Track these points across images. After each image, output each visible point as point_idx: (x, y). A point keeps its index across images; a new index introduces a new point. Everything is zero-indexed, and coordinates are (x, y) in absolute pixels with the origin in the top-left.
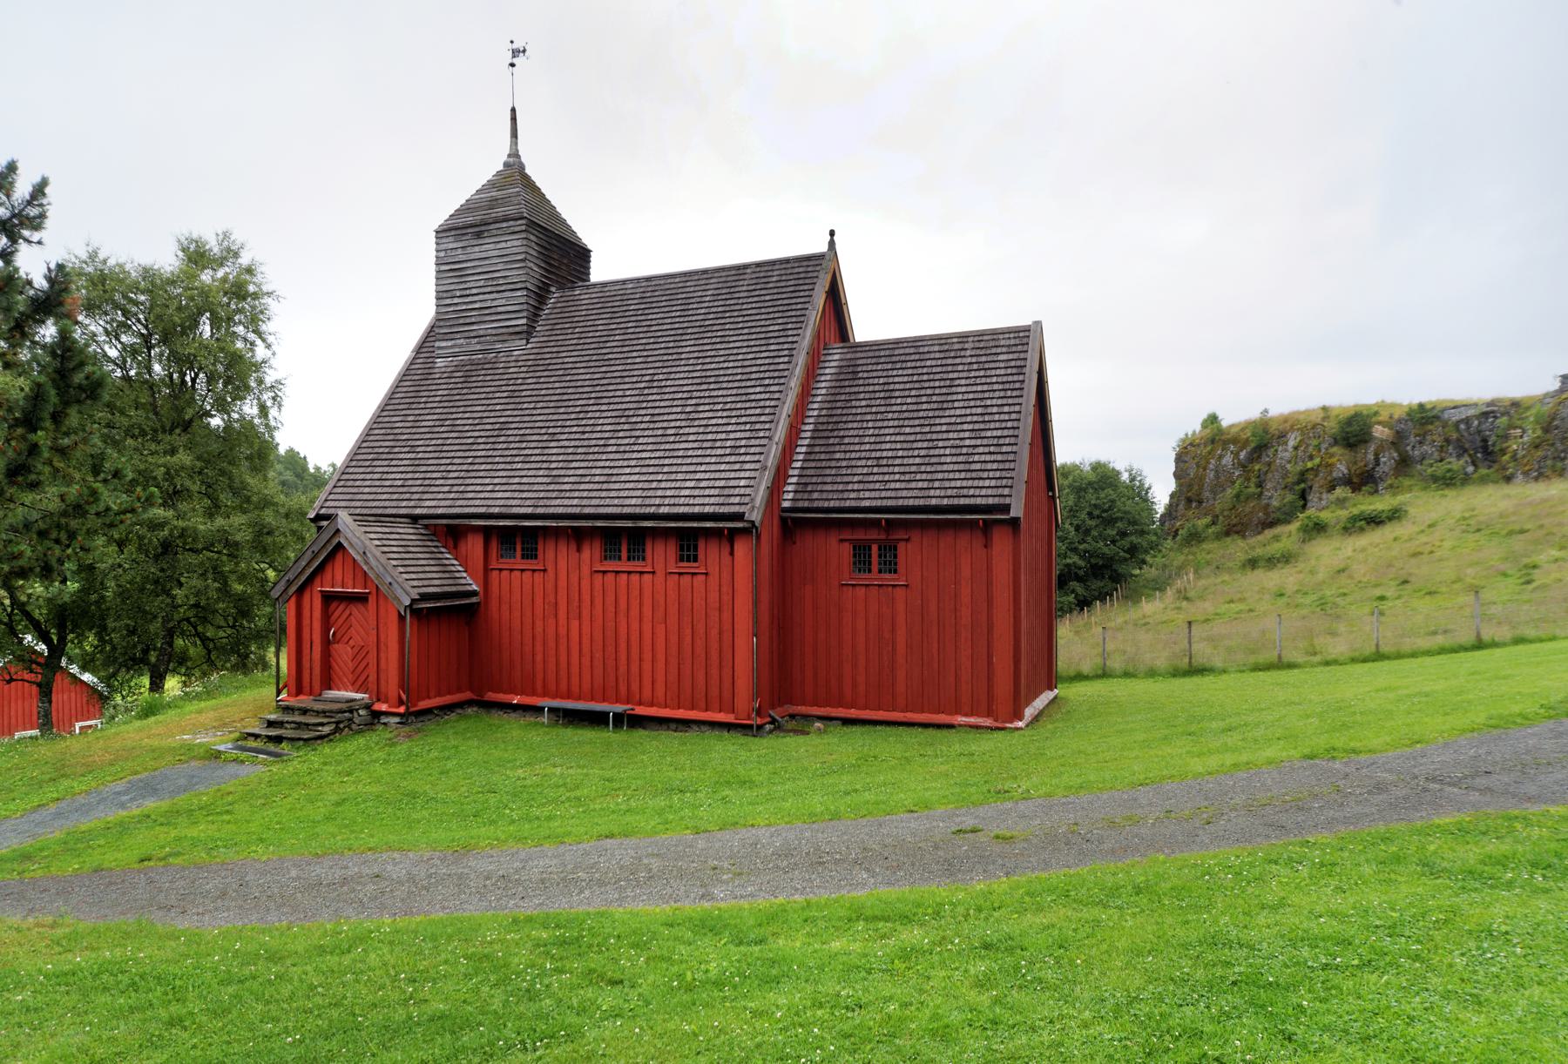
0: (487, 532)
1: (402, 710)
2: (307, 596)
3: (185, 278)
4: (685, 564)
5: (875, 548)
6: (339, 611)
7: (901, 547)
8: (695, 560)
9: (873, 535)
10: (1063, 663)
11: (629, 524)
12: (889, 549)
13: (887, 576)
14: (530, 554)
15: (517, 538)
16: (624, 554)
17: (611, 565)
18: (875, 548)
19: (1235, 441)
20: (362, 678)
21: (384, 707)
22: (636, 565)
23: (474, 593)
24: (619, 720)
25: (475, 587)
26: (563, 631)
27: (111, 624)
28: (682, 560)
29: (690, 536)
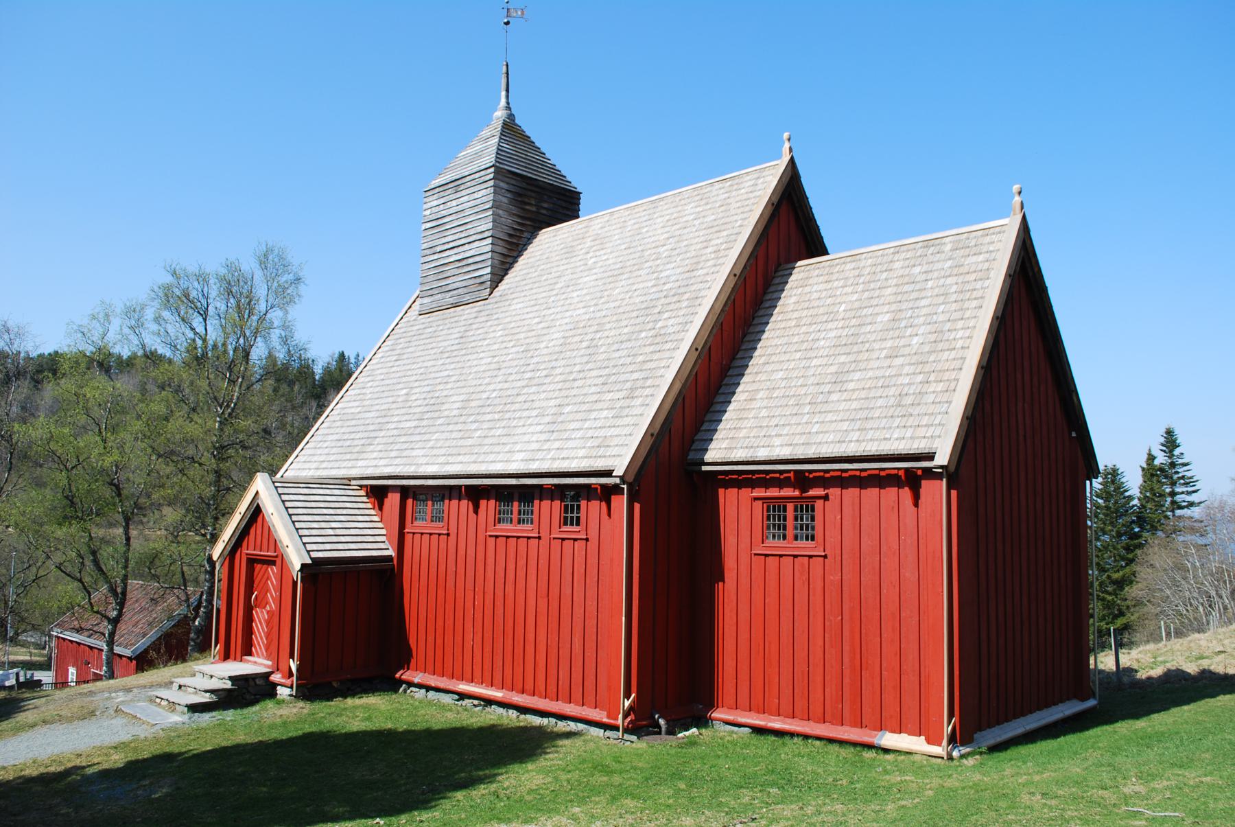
4: (568, 528)
5: (790, 507)
12: (806, 506)
13: (802, 543)
16: (515, 516)
18: (790, 507)
22: (526, 529)
23: (389, 558)
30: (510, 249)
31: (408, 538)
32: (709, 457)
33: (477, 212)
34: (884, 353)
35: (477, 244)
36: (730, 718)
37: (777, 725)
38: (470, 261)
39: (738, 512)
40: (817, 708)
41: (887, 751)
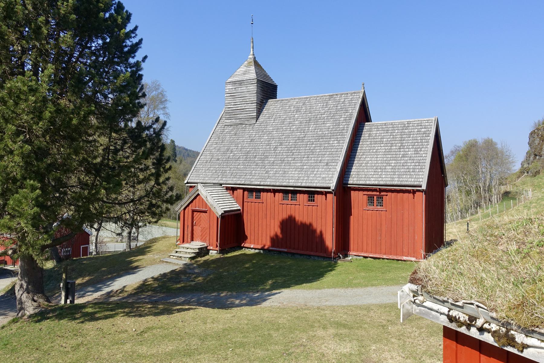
0: (244, 189)
2: (187, 209)
4: (310, 202)
5: (375, 197)
6: (195, 213)
7: (384, 197)
8: (314, 201)
10: (448, 237)
11: (292, 189)
12: (380, 197)
13: (379, 207)
14: (258, 197)
15: (256, 191)
16: (290, 198)
17: (285, 202)
18: (375, 197)
20: (204, 238)
21: (211, 248)
22: (294, 202)
23: (239, 210)
24: (287, 253)
27: (119, 213)
28: (309, 201)
29: (312, 193)
30: (261, 105)
31: (245, 203)
32: (350, 182)
33: (251, 92)
34: (401, 156)
35: (250, 105)
36: (357, 254)
37: (395, 258)
38: (247, 110)
39: (358, 199)
40: (384, 251)
41: (405, 261)
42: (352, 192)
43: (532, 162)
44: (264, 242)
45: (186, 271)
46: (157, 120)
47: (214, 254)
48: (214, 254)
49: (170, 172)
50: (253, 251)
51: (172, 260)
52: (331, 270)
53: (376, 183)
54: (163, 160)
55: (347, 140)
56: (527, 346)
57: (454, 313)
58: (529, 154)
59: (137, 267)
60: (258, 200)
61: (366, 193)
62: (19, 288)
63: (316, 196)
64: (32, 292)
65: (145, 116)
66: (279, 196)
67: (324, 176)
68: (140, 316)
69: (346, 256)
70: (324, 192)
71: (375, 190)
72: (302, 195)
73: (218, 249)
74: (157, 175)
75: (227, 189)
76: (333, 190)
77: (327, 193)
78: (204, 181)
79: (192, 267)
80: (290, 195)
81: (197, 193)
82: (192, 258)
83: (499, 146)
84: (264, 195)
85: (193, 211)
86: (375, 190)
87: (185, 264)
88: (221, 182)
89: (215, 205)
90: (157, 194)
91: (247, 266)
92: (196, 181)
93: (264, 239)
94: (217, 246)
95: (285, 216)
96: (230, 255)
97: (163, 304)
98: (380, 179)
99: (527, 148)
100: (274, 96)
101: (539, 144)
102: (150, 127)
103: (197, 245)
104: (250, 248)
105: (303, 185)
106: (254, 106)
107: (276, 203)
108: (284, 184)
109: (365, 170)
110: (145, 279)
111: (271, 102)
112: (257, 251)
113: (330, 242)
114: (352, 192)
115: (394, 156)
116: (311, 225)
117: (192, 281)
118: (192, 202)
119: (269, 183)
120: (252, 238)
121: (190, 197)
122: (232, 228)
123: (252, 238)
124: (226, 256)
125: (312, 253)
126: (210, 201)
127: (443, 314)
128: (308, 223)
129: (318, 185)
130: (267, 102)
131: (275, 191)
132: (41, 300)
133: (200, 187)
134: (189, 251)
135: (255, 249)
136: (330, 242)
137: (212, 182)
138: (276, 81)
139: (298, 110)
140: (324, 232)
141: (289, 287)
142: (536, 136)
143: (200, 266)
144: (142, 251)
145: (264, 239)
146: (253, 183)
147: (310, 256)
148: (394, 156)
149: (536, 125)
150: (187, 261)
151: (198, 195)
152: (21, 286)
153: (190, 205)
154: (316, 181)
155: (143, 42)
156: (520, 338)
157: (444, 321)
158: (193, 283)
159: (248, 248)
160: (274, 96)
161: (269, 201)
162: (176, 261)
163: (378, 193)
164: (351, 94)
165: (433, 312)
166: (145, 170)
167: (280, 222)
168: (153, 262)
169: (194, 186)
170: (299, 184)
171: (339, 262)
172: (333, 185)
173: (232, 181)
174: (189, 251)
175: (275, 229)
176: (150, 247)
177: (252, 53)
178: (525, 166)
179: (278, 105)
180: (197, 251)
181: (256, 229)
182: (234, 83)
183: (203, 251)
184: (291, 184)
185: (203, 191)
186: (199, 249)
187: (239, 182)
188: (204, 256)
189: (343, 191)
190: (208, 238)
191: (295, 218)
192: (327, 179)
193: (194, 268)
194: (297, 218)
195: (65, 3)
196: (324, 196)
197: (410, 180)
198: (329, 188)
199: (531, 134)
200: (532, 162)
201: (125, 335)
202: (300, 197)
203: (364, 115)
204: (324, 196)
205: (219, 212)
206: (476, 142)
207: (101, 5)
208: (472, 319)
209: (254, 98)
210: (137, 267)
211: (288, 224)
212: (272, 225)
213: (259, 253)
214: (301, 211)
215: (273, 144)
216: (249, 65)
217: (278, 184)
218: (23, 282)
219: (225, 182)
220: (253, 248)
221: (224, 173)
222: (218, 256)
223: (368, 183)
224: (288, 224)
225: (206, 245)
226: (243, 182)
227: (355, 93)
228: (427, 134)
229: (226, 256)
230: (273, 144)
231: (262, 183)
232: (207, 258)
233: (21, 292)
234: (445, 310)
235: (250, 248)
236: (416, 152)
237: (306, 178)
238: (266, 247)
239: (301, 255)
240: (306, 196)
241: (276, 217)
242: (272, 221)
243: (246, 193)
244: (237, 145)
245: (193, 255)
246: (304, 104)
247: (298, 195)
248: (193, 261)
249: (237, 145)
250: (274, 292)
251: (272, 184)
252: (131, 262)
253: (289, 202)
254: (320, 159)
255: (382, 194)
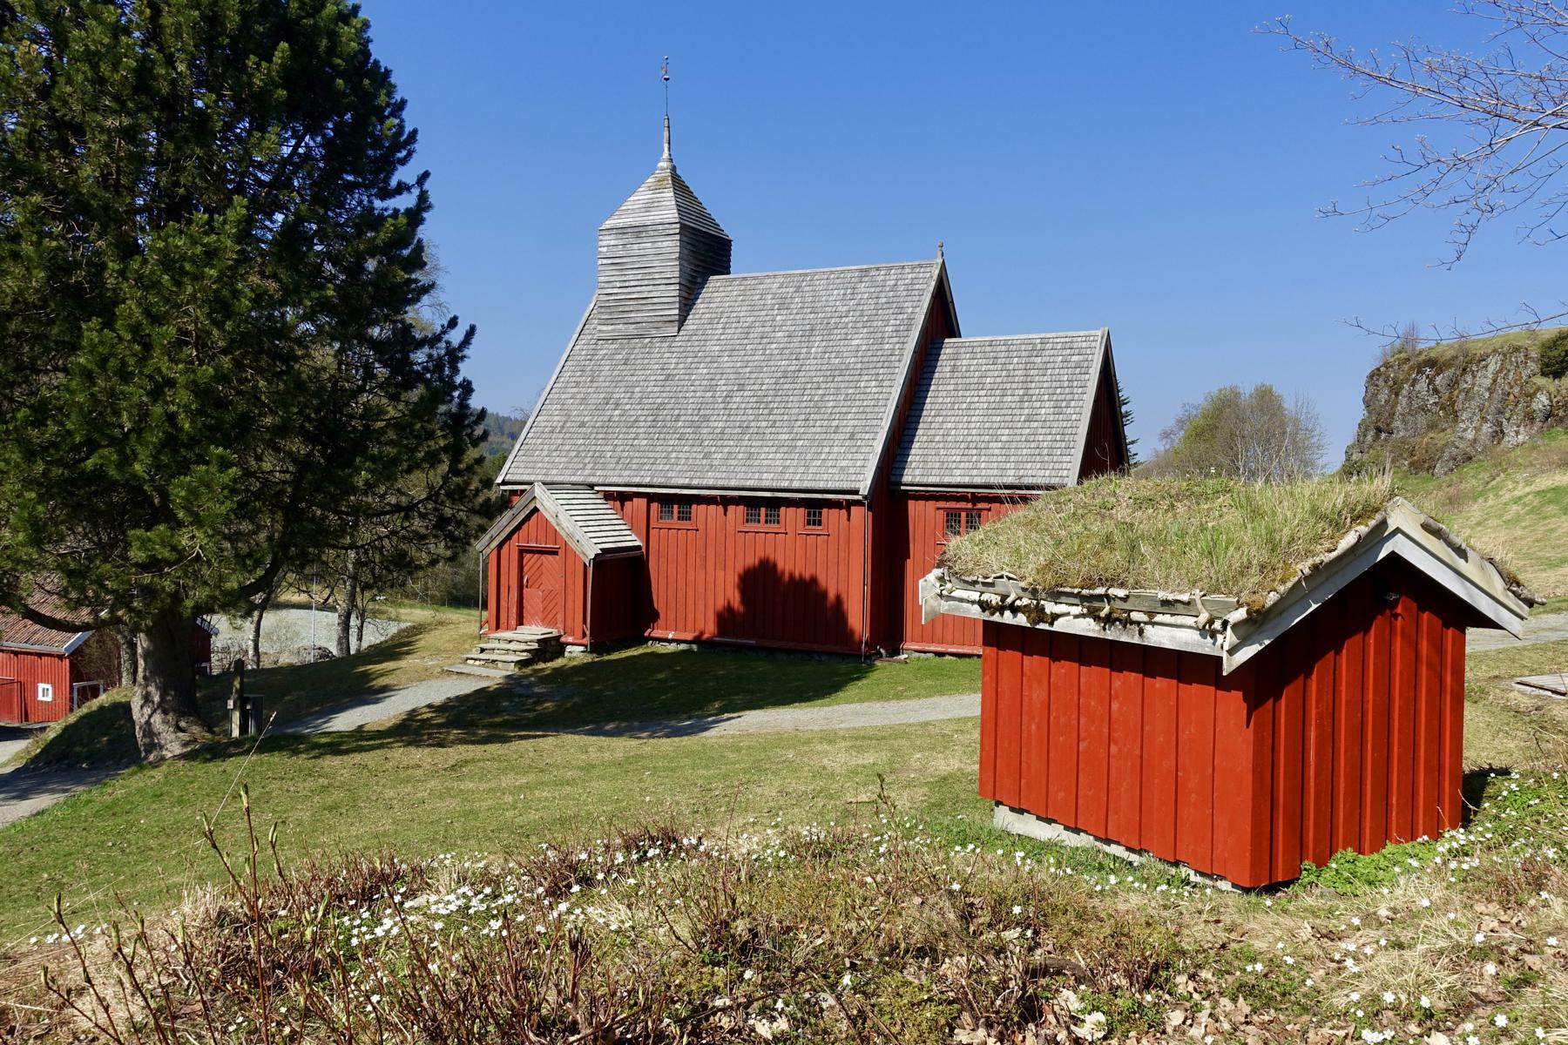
0: (651, 498)
1: (84, 615)
2: (506, 547)
3: (793, 733)
5: (963, 514)
6: (527, 557)
9: (962, 505)
14: (684, 516)
18: (963, 514)
19: (1432, 363)
21: (570, 639)
22: (773, 527)
23: (639, 548)
25: (638, 543)
26: (710, 579)
29: (815, 505)
32: (906, 479)
33: (665, 256)
42: (911, 503)
43: (1371, 447)
44: (700, 626)
45: (510, 690)
46: (453, 323)
47: (576, 653)
48: (576, 653)
49: (482, 445)
50: (672, 647)
51: (472, 668)
52: (858, 679)
53: (966, 480)
54: (466, 416)
55: (900, 380)
56: (1055, 617)
57: (985, 597)
58: (1363, 427)
59: (385, 689)
60: (685, 524)
61: (941, 504)
62: (141, 702)
63: (825, 511)
64: (175, 711)
65: (424, 315)
66: (737, 512)
67: (844, 463)
68: (441, 745)
69: (895, 651)
70: (840, 502)
71: (963, 498)
72: (791, 510)
73: (587, 640)
74: (456, 451)
75: (608, 496)
76: (865, 497)
77: (850, 504)
78: (549, 479)
79: (525, 682)
80: (763, 510)
81: (531, 507)
82: (522, 664)
83: (1289, 405)
84: (698, 510)
85: (522, 551)
86: (963, 498)
87: (508, 677)
88: (592, 480)
89: (579, 534)
90: (458, 495)
91: (660, 676)
92: (525, 478)
93: (700, 617)
94: (584, 635)
95: (751, 560)
96: (615, 656)
97: (484, 727)
98: (975, 472)
99: (1359, 413)
100: (725, 270)
101: (1387, 402)
102: (437, 338)
103: (533, 632)
104: (669, 637)
105: (796, 485)
106: (674, 290)
107: (730, 530)
108: (749, 483)
109: (942, 452)
110: (410, 708)
111: (715, 281)
112: (683, 647)
113: (858, 619)
114: (911, 503)
115: (1008, 418)
116: (814, 580)
117: (528, 710)
118: (518, 528)
119: (711, 483)
120: (672, 615)
121: (514, 516)
122: (621, 589)
123: (672, 615)
124: (606, 658)
125: (815, 647)
126: (565, 525)
127: (973, 602)
128: (807, 576)
129: (830, 485)
130: (705, 281)
131: (726, 502)
132: (196, 729)
133: (539, 490)
134: (513, 646)
135: (679, 642)
136: (858, 619)
137: (567, 479)
138: (729, 230)
139: (783, 305)
140: (844, 597)
141: (761, 707)
142: (1381, 383)
143: (545, 679)
144: (391, 650)
145: (700, 617)
146: (673, 482)
147: (810, 653)
148: (1008, 418)
149: (1385, 355)
150: (512, 670)
151: (536, 510)
152: (147, 698)
153: (515, 537)
154: (825, 477)
155: (419, 137)
156: (1050, 607)
157: (975, 612)
158: (531, 715)
159: (660, 640)
160: (725, 270)
161: (711, 524)
162: (484, 672)
163: (970, 505)
164: (913, 268)
165: (965, 605)
166: (379, 456)
167: (740, 577)
168: (424, 675)
169: (523, 491)
170: (785, 484)
171: (878, 663)
172: (864, 486)
173: (618, 477)
174: (513, 646)
175: (728, 593)
176: (409, 643)
177: (666, 154)
178: (1354, 457)
179: (735, 290)
180: (536, 646)
181: (680, 594)
182: (621, 231)
183: (550, 648)
184: (765, 484)
185: (548, 502)
186: (539, 641)
187: (637, 480)
188: (551, 660)
189: (889, 499)
190: (560, 617)
191: (775, 565)
192: (852, 470)
193: (531, 685)
194: (780, 565)
195: (264, 64)
196: (844, 512)
197: (1042, 473)
198: (856, 492)
199: (1371, 377)
200: (1371, 447)
201: (419, 772)
202: (787, 513)
203: (941, 321)
204: (844, 512)
205: (590, 551)
206: (1237, 395)
207: (339, 61)
208: (1004, 597)
209: (672, 270)
210: (385, 689)
211: (760, 580)
212: (720, 581)
213: (689, 651)
214: (791, 548)
215: (723, 387)
216: (658, 188)
217: (733, 483)
218: (152, 689)
219: (601, 481)
220: (672, 641)
221: (598, 459)
222: (589, 658)
223: (947, 480)
224: (760, 580)
225: (555, 633)
226: (647, 480)
227: (920, 266)
228: (1082, 368)
229: (606, 658)
230: (723, 387)
231: (695, 482)
232: (558, 663)
233: (147, 711)
234: (975, 596)
235: (669, 637)
236: (1058, 411)
237: (801, 470)
238: (706, 636)
239: (789, 652)
240: (802, 511)
241: (730, 564)
242: (720, 573)
243: (654, 506)
244: (629, 389)
245: (525, 656)
246: (798, 289)
247: (783, 509)
248: (528, 671)
249: (629, 389)
250: (726, 715)
251: (721, 483)
252: (366, 676)
253: (761, 527)
254: (835, 423)
255: (980, 506)
